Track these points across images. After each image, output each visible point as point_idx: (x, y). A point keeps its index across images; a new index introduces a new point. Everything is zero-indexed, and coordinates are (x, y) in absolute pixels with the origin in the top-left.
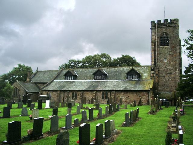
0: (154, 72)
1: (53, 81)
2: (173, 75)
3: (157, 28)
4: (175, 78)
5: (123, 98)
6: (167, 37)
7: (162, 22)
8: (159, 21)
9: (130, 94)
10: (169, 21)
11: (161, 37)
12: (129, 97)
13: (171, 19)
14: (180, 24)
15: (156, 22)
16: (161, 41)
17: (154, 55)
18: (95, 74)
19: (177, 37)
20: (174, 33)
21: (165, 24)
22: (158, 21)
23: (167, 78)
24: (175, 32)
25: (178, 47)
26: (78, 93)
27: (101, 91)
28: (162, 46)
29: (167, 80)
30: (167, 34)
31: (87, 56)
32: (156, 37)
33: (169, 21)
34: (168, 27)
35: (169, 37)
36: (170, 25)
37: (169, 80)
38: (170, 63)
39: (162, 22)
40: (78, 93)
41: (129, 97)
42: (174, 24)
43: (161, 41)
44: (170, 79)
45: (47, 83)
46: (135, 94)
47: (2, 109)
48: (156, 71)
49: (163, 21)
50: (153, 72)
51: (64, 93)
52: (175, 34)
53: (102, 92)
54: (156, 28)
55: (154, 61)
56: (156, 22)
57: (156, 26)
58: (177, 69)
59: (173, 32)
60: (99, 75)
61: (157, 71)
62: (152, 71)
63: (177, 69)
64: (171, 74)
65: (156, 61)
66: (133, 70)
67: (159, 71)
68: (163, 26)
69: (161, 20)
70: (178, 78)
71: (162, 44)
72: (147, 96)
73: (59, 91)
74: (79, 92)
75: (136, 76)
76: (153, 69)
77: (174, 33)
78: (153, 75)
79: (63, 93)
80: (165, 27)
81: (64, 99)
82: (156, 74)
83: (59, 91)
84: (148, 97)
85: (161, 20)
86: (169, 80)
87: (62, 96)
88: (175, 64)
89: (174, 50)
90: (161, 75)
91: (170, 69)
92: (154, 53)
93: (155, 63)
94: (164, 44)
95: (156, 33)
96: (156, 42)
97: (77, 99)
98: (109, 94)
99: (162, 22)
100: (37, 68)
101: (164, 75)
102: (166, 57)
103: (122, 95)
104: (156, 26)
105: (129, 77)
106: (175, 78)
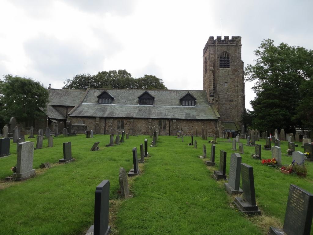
0: (214, 98)
1: (81, 104)
2: (235, 103)
3: (217, 45)
4: (237, 106)
5: (186, 128)
6: (228, 58)
7: (222, 39)
8: (219, 38)
9: (194, 124)
10: (230, 38)
11: (221, 58)
12: (192, 127)
13: (232, 37)
14: (243, 42)
15: (215, 38)
16: (220, 62)
17: (214, 78)
18: (99, 97)
19: (240, 59)
20: (236, 54)
21: (226, 42)
22: (218, 37)
23: (228, 106)
24: (237, 52)
25: (240, 71)
26: (125, 122)
27: (157, 119)
28: (222, 67)
29: (228, 108)
30: (228, 54)
31: (99, 72)
32: (215, 56)
33: (230, 38)
34: (229, 45)
35: (230, 57)
36: (231, 43)
37: (230, 108)
38: (230, 89)
39: (222, 39)
40: (125, 122)
41: (192, 127)
42: (236, 42)
43: (220, 62)
44: (231, 108)
45: (74, 107)
46: (200, 124)
47: (131, 151)
48: (216, 97)
49: (224, 37)
50: (212, 98)
51: (170, 123)
52: (237, 54)
53: (158, 121)
54: (215, 45)
55: (214, 85)
56: (215, 38)
57: (216, 42)
58: (240, 97)
59: (235, 52)
60: (104, 97)
61: (217, 97)
62: (211, 97)
63: (240, 97)
64: (231, 101)
65: (216, 86)
66: (146, 94)
67: (219, 97)
68: (224, 44)
69: (228, 36)
70: (241, 107)
71: (222, 65)
72: (215, 126)
73: (99, 118)
74: (128, 120)
75: (110, 100)
76: (212, 94)
77: (236, 54)
78: (213, 102)
79: (104, 121)
80: (226, 45)
81: (105, 128)
82: (216, 101)
83: (99, 118)
84: (216, 128)
85: (228, 36)
86: (230, 108)
87: (103, 124)
88: (237, 90)
89: (236, 74)
90: (221, 102)
91: (231, 96)
92: (214, 76)
93: (215, 88)
94: (225, 66)
95: (216, 51)
96: (216, 63)
97: (125, 129)
98: (168, 123)
99: (223, 38)
100: (50, 85)
101: (224, 102)
102: (227, 81)
103: (184, 125)
104: (216, 42)
105: (100, 101)
106: (237, 106)
